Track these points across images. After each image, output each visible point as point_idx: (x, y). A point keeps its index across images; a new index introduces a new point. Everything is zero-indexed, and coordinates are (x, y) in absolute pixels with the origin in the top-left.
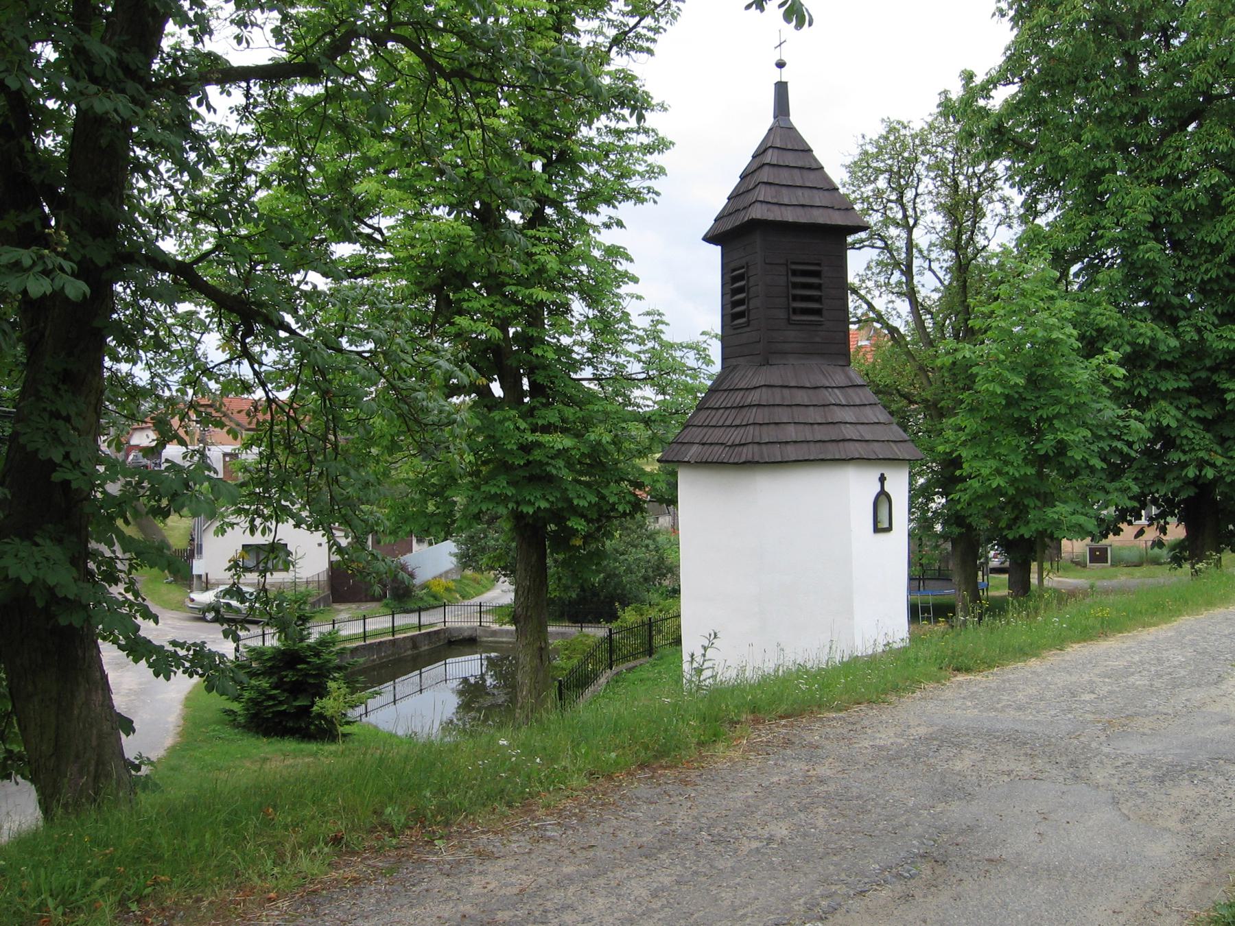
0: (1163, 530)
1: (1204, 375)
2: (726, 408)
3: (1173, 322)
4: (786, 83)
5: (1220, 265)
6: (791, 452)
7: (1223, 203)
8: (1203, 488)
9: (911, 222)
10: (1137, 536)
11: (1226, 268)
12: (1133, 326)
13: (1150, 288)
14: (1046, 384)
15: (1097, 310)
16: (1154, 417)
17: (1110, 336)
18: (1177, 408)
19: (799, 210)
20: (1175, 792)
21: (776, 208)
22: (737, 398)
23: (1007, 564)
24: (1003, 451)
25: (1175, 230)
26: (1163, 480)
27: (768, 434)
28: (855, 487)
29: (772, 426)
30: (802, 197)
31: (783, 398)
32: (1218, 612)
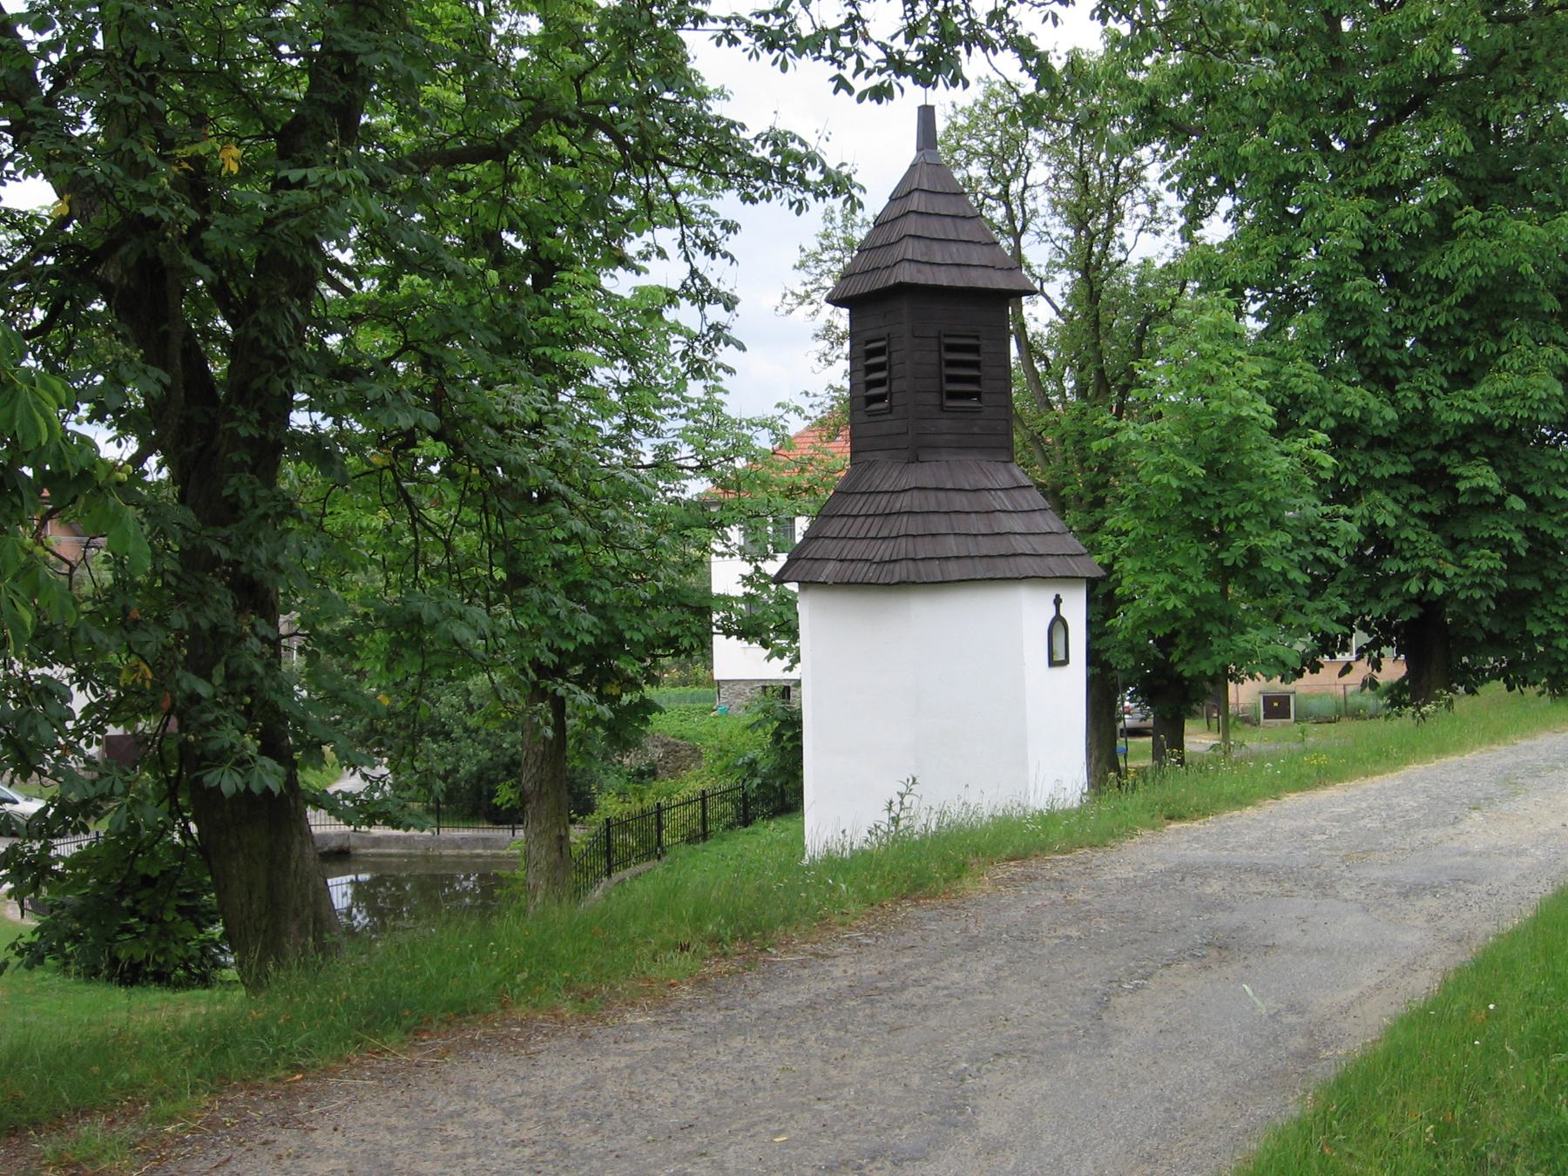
0: (1377, 665)
1: (1429, 455)
2: (867, 516)
3: (1390, 384)
4: (932, 108)
5: (1450, 309)
6: (954, 570)
7: (1455, 226)
8: (1430, 607)
9: (1019, 225)
10: (1341, 674)
11: (1458, 311)
12: (1337, 391)
13: (1359, 340)
14: (1234, 474)
15: (1290, 369)
16: (1366, 513)
17: (1309, 403)
18: (1396, 500)
19: (954, 271)
20: (1419, 904)
21: (927, 268)
22: (882, 503)
23: (1150, 722)
24: (1178, 562)
25: (1391, 260)
26: (1378, 598)
27: (925, 548)
28: (1029, 610)
29: (928, 539)
30: (957, 253)
31: (938, 503)
32: (1452, 760)
